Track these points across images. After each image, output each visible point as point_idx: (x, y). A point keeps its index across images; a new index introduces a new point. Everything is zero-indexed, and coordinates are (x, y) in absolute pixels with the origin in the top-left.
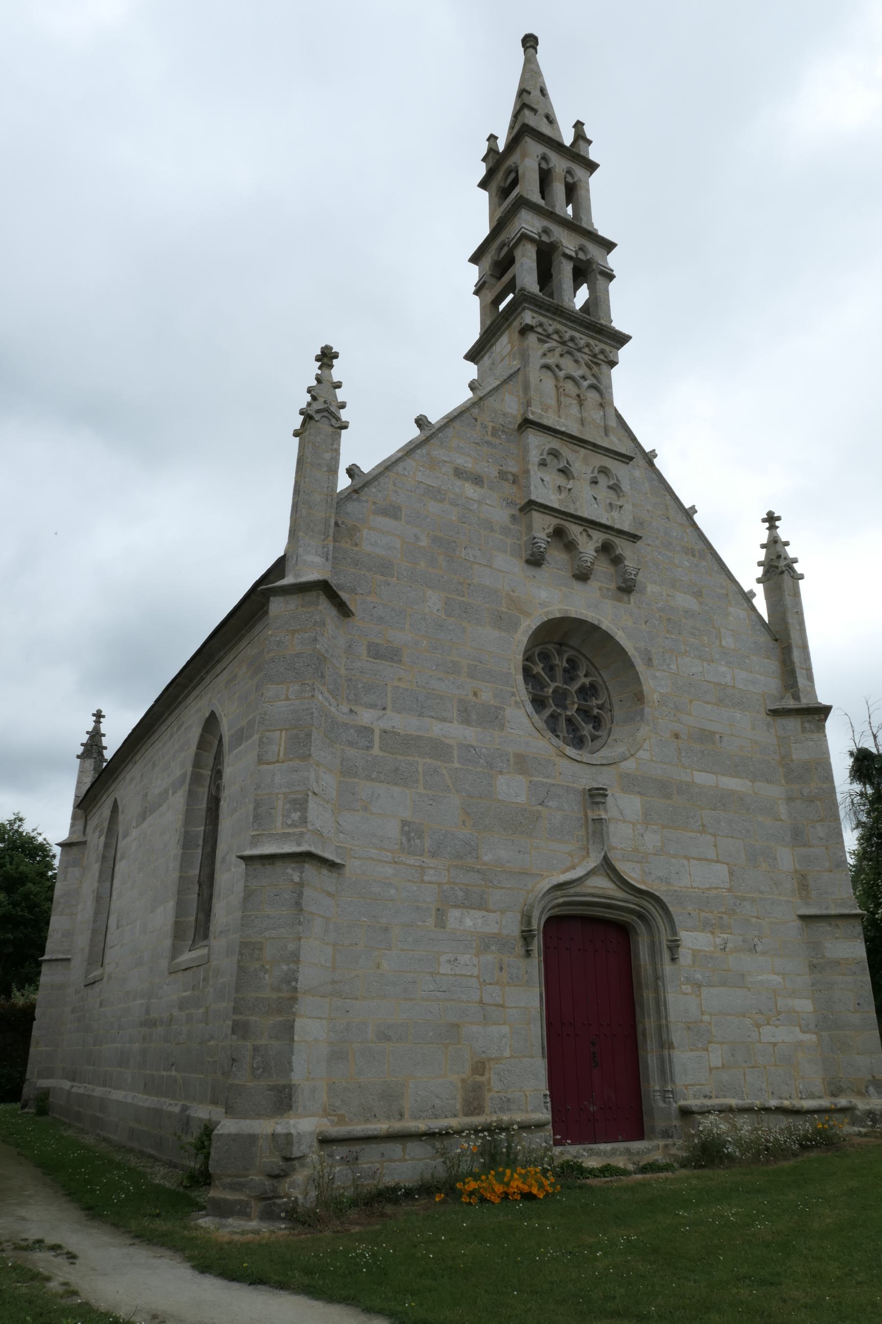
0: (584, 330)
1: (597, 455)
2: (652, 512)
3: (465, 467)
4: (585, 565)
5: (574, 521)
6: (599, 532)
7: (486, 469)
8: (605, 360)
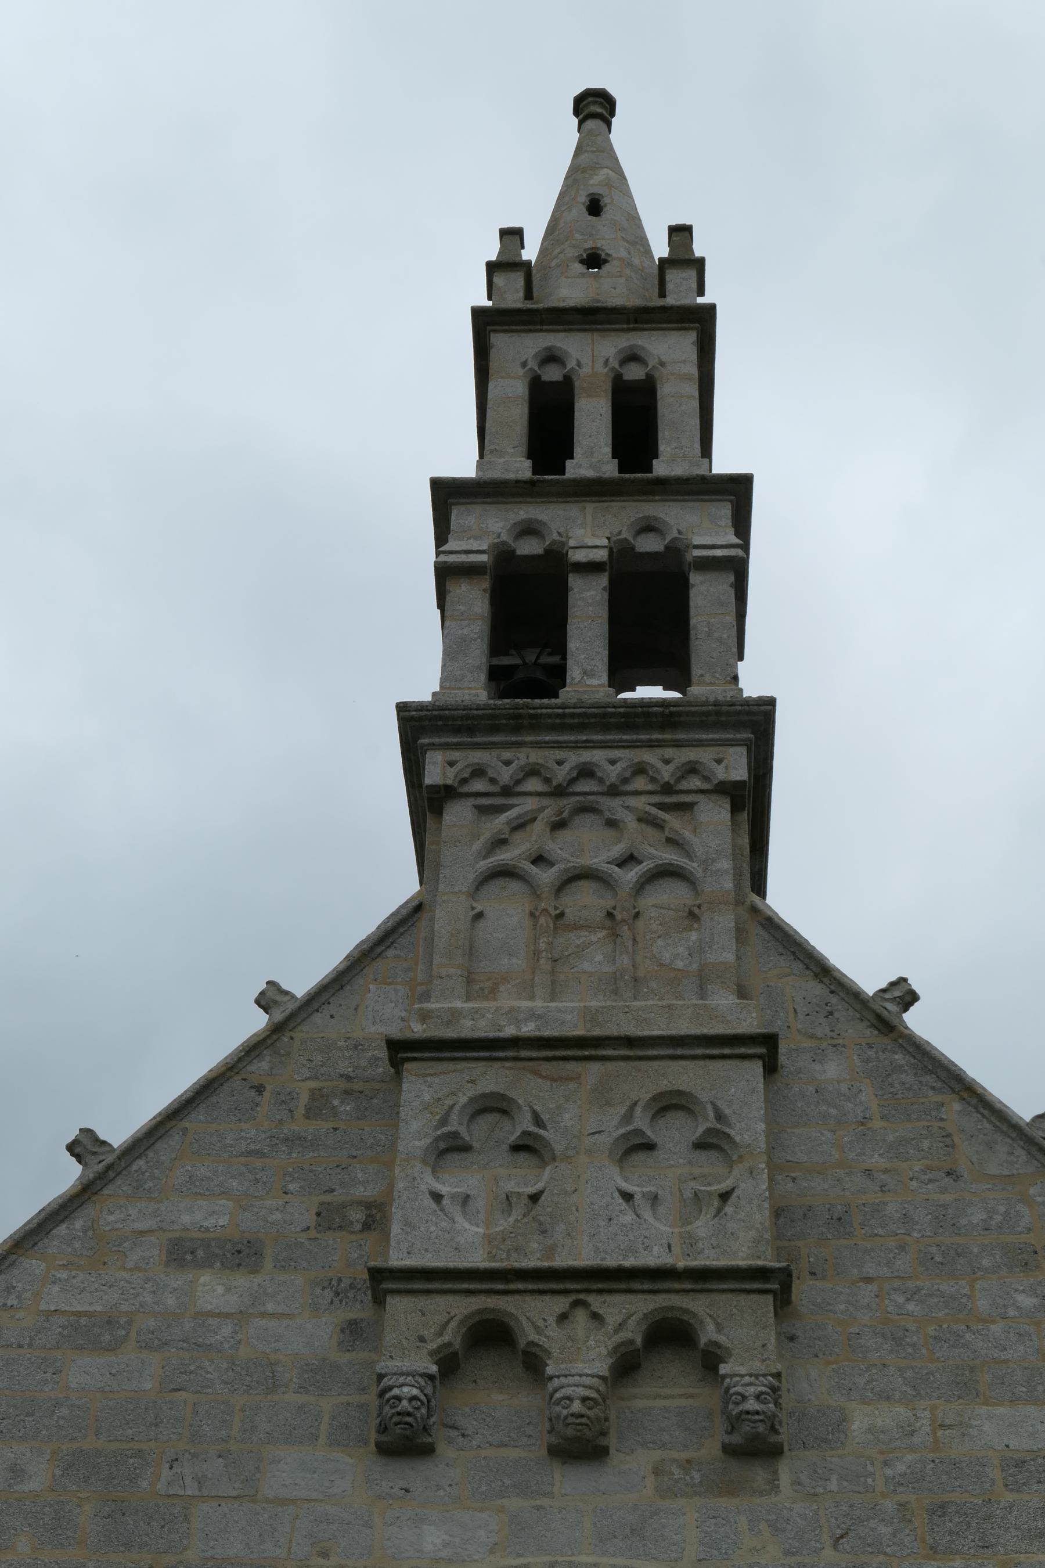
0: (617, 737)
1: (643, 1065)
2: (886, 1171)
3: (207, 1229)
4: (565, 1412)
5: (530, 1286)
6: (630, 1297)
7: (277, 1216)
8: (706, 786)
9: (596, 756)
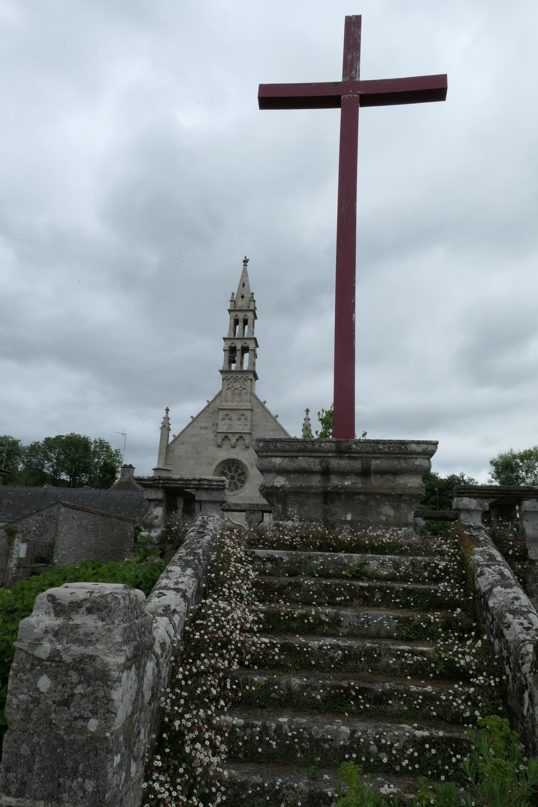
9: (238, 375)
